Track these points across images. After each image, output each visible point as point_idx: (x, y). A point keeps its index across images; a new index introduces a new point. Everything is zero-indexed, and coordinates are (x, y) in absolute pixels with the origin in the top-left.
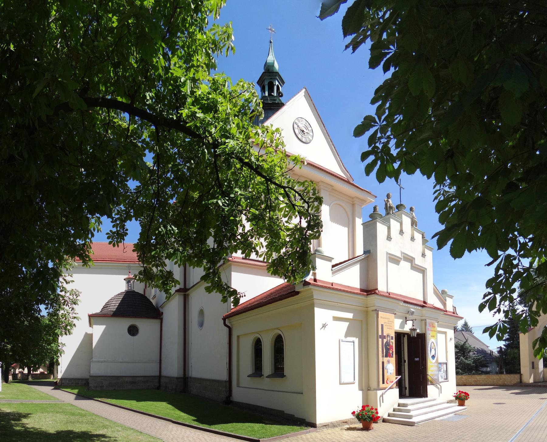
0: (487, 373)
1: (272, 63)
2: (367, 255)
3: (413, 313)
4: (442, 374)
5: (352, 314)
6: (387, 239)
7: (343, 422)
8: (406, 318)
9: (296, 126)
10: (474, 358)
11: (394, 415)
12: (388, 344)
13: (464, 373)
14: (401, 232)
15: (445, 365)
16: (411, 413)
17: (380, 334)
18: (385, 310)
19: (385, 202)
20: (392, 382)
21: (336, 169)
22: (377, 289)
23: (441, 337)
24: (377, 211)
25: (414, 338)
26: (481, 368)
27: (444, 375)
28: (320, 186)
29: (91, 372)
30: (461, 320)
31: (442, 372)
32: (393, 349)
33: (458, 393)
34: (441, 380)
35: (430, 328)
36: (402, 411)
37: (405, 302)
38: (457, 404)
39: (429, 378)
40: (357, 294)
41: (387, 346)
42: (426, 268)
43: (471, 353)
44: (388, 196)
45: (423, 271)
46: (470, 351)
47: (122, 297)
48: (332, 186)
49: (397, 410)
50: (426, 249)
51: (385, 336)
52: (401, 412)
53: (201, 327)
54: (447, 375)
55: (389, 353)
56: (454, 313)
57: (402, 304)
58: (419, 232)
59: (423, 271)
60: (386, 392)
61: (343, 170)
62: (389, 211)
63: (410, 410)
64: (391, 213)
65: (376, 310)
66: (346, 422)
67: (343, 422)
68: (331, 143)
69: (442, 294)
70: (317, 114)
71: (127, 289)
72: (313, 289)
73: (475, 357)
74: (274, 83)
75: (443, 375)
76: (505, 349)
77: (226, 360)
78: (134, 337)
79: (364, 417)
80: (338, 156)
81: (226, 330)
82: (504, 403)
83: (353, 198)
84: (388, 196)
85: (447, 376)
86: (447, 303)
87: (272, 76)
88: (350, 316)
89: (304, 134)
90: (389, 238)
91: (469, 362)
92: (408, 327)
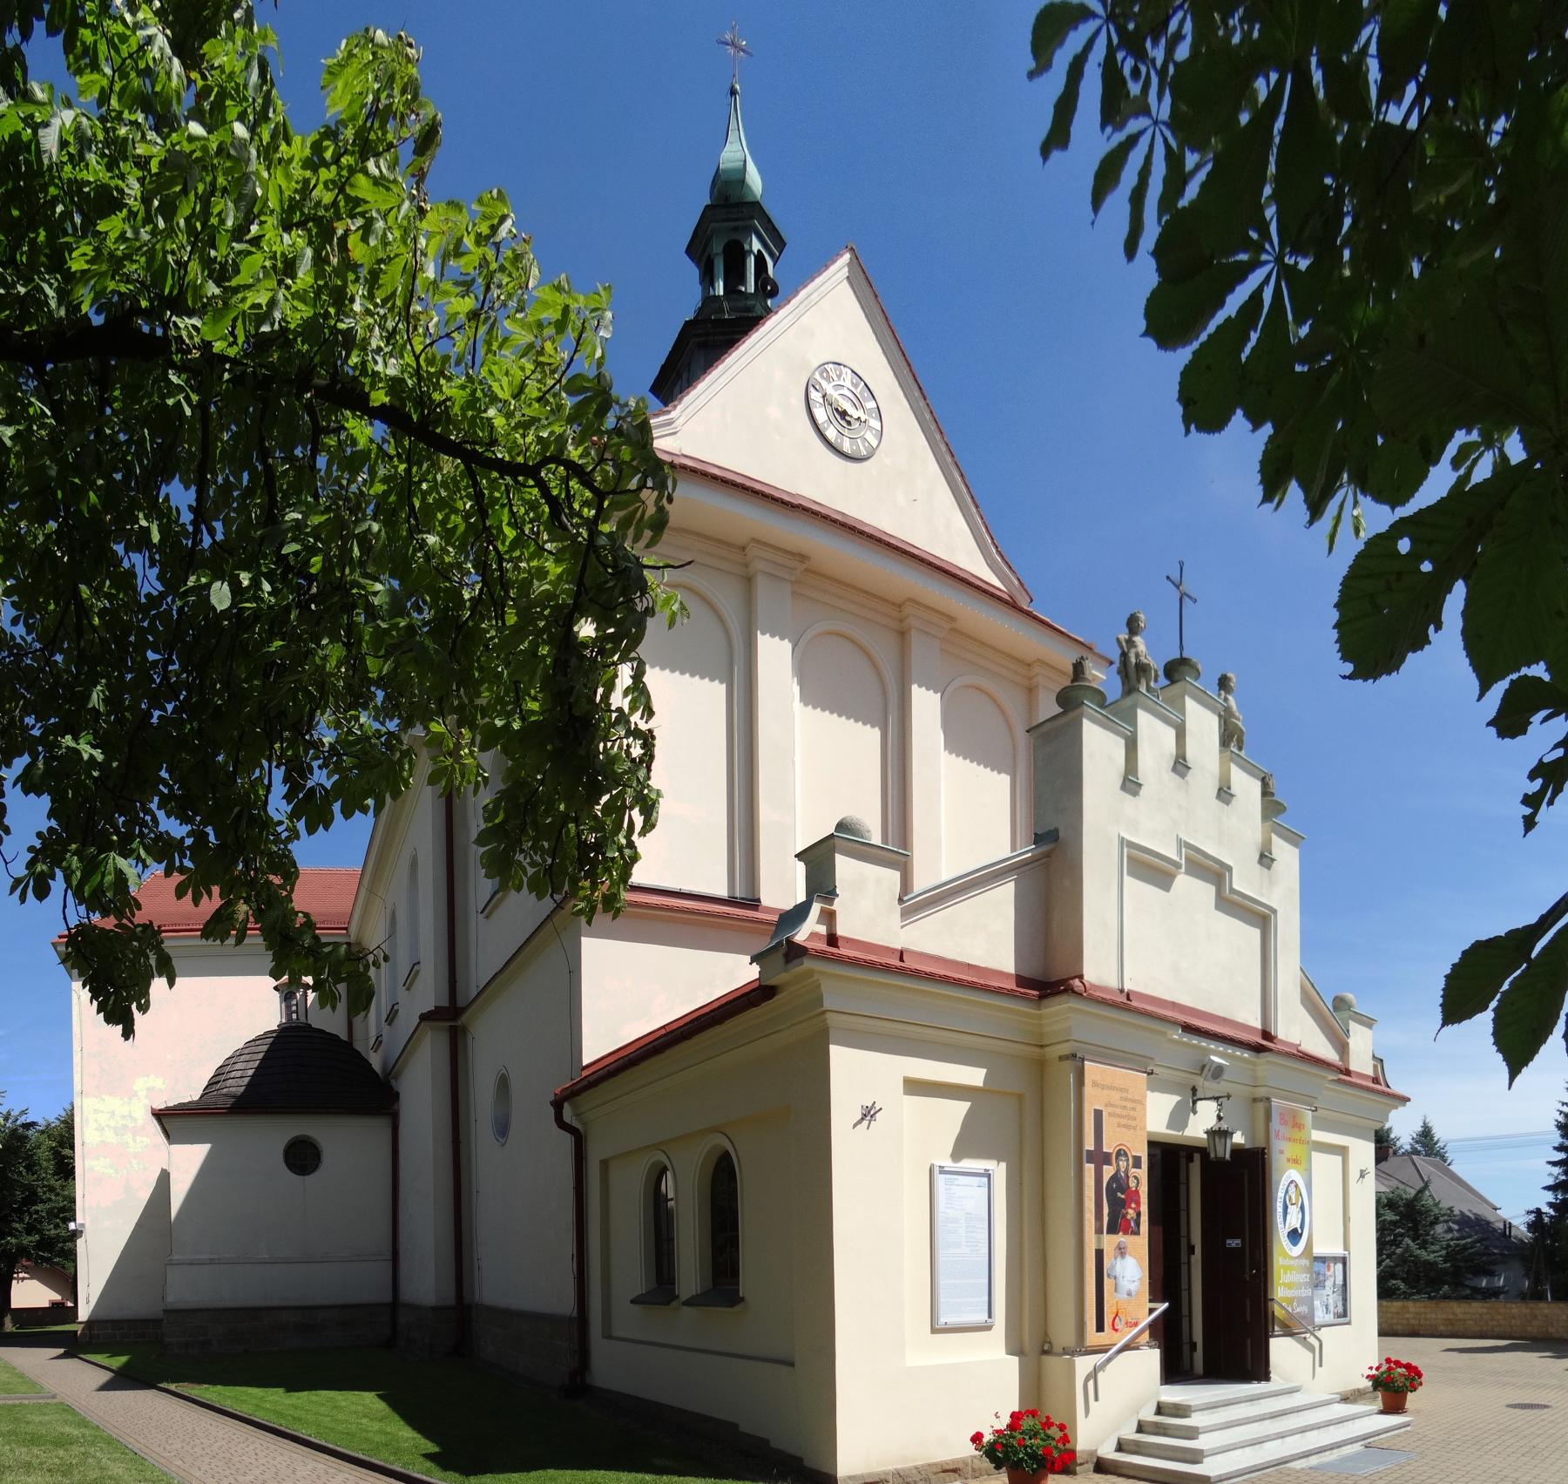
0: (1491, 1294)
1: (736, 170)
2: (1044, 849)
3: (1218, 1072)
4: (1328, 1295)
5: (985, 1070)
6: (1124, 787)
7: (944, 1471)
8: (1194, 1090)
9: (815, 396)
10: (1449, 1246)
11: (1138, 1448)
12: (1119, 1184)
13: (1413, 1294)
14: (1181, 765)
15: (1340, 1266)
16: (1200, 1443)
17: (1089, 1145)
18: (1111, 1057)
19: (1121, 647)
20: (1136, 1324)
21: (969, 558)
22: (1081, 977)
23: (1325, 1167)
24: (1085, 679)
25: (1221, 1162)
26: (1470, 1276)
27: (1334, 1299)
28: (907, 618)
29: (170, 1299)
30: (1401, 1109)
31: (1329, 1290)
32: (1138, 1204)
33: (1384, 1368)
34: (1320, 1316)
35: (1283, 1130)
36: (1170, 1432)
37: (1188, 1029)
38: (1379, 1405)
39: (1278, 1312)
40: (1009, 994)
41: (1117, 1196)
42: (1274, 906)
43: (1439, 1229)
44: (1133, 625)
45: (1261, 918)
46: (1436, 1221)
47: (265, 1048)
48: (951, 619)
49: (1150, 1429)
50: (1274, 837)
51: (1108, 1155)
52: (1165, 1435)
53: (503, 1137)
54: (1345, 1300)
55: (1124, 1216)
56: (1375, 1080)
57: (1177, 1035)
58: (1293, 838)
59: (1261, 918)
60: (1109, 1360)
61: (995, 561)
62: (1133, 681)
63: (1197, 1428)
64: (1143, 689)
65: (1074, 1056)
66: (955, 1471)
67: (944, 1471)
68: (949, 459)
69: (1335, 1008)
70: (897, 348)
71: (284, 1021)
72: (821, 973)
73: (1452, 1239)
74: (747, 247)
75: (1331, 1301)
76: (1551, 1217)
77: (570, 1248)
78: (306, 1177)
79: (1016, 1453)
80: (977, 507)
81: (567, 1139)
82: (1546, 1407)
83: (1029, 665)
84: (1133, 625)
85: (1345, 1305)
86: (1352, 1042)
87: (737, 220)
88: (975, 1076)
89: (849, 423)
90: (1131, 784)
91: (1432, 1256)
92: (1201, 1123)
